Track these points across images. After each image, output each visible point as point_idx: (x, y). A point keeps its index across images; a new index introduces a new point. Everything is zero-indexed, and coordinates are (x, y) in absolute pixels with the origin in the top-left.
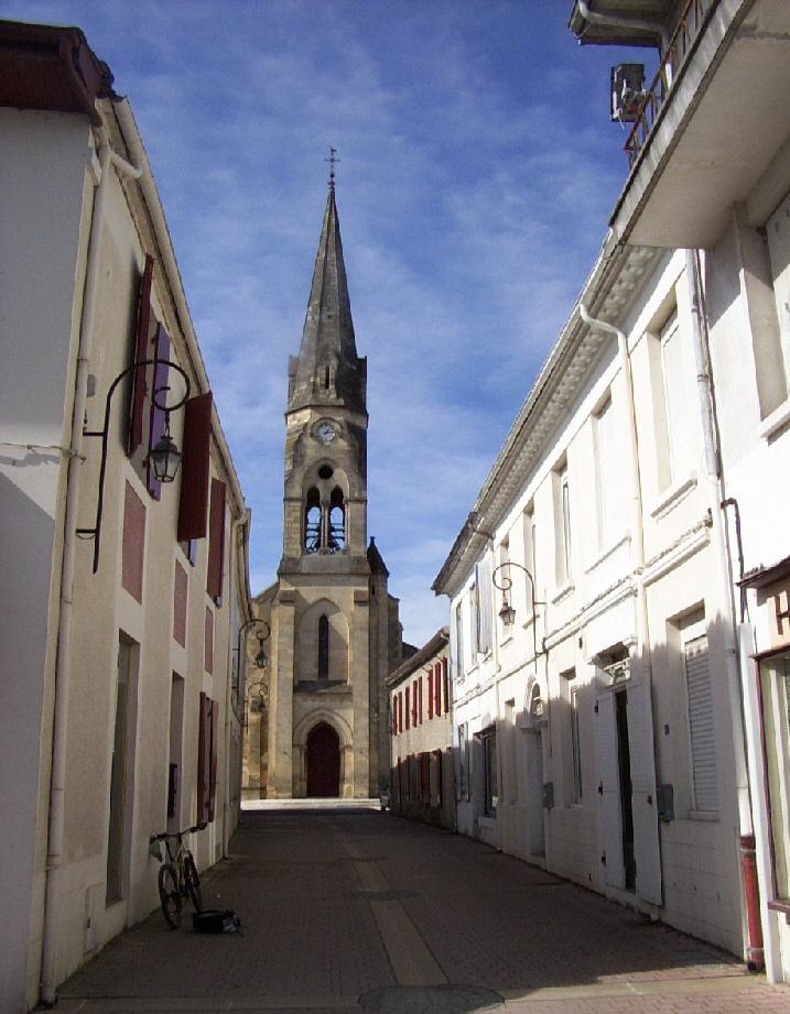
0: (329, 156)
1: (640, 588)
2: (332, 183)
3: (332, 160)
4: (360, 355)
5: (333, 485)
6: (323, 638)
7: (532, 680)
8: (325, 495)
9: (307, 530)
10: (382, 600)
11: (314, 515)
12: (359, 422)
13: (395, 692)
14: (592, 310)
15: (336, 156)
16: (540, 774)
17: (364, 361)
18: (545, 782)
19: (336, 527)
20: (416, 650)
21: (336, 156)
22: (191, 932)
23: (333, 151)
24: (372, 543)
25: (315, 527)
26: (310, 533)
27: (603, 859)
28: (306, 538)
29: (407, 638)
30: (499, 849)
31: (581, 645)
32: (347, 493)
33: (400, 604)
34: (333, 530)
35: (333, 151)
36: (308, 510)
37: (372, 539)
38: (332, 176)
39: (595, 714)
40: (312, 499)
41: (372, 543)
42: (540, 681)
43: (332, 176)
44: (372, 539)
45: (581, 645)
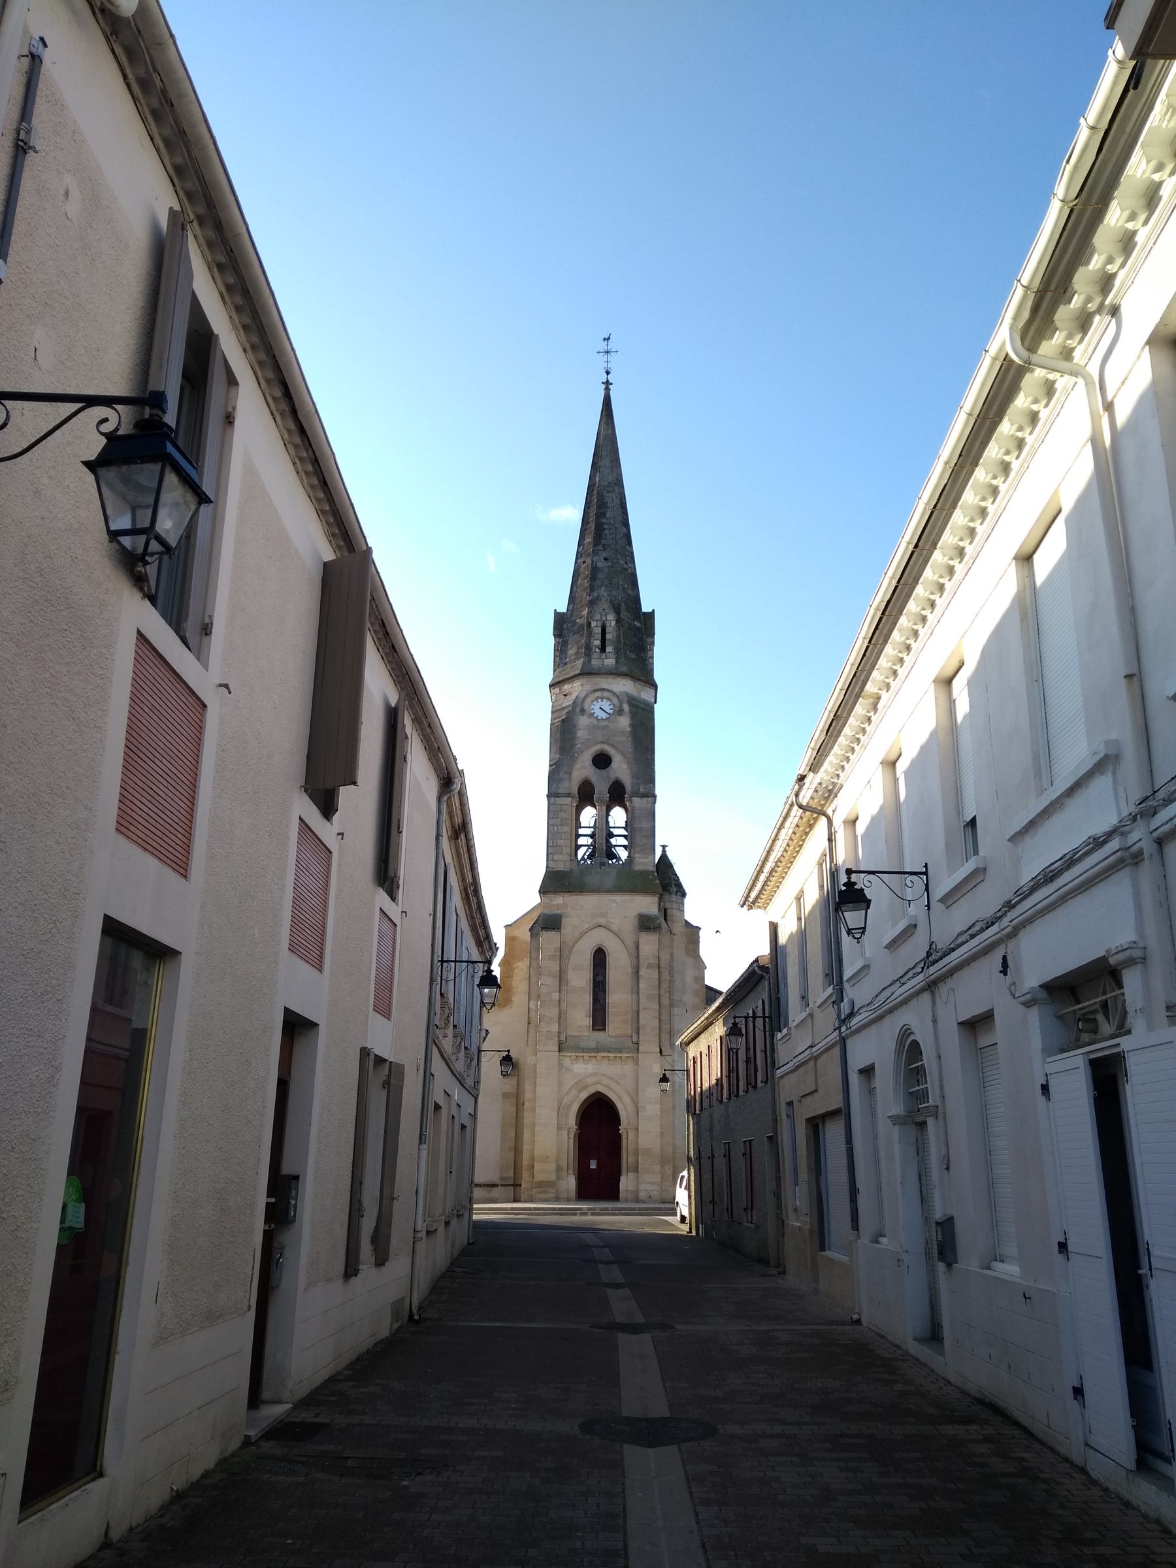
0: (603, 346)
1: (1147, 846)
2: (607, 383)
3: (608, 352)
4: (646, 608)
5: (613, 777)
6: (600, 978)
7: (906, 1032)
8: (602, 789)
9: (578, 836)
10: (678, 928)
11: (588, 816)
12: (646, 695)
13: (693, 1050)
14: (1027, 343)
15: (612, 346)
16: (924, 1199)
17: (651, 616)
18: (938, 1215)
19: (616, 832)
20: (720, 993)
21: (612, 346)
22: (1130, 962)
23: (898, 1260)
24: (664, 851)
25: (589, 831)
26: (581, 841)
27: (1078, 1392)
28: (578, 847)
29: (709, 981)
30: (855, 1317)
31: (1004, 971)
32: (628, 788)
33: (701, 933)
34: (612, 835)
35: (898, 1260)
36: (579, 810)
37: (664, 847)
38: (608, 373)
39: (1041, 1099)
40: (586, 796)
41: (664, 851)
42: (923, 1036)
43: (608, 373)
44: (664, 847)
45: (1004, 971)
